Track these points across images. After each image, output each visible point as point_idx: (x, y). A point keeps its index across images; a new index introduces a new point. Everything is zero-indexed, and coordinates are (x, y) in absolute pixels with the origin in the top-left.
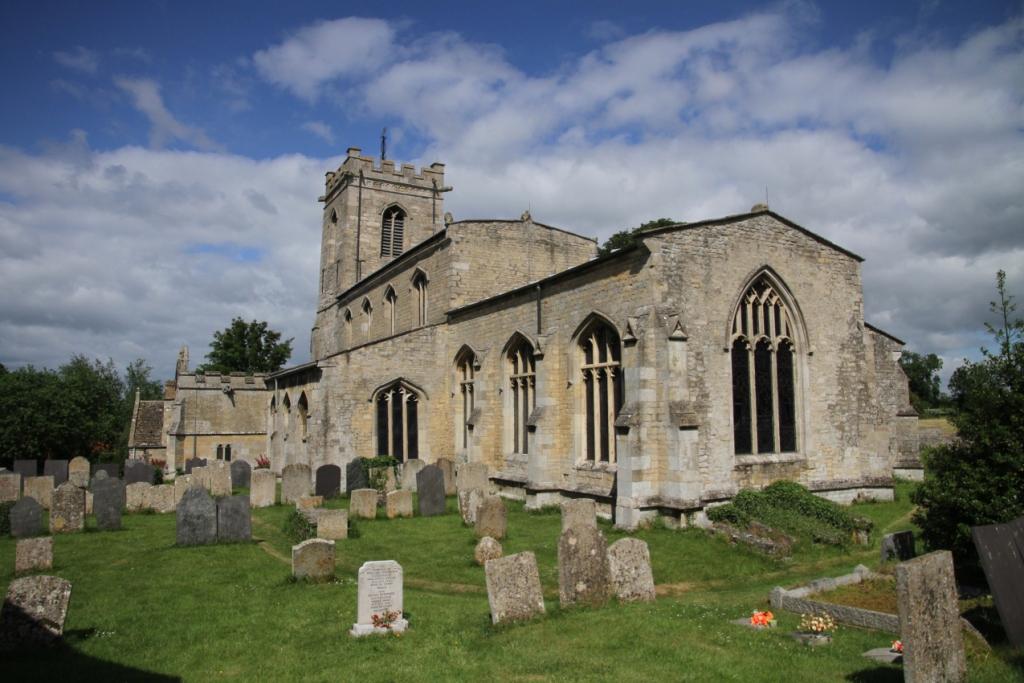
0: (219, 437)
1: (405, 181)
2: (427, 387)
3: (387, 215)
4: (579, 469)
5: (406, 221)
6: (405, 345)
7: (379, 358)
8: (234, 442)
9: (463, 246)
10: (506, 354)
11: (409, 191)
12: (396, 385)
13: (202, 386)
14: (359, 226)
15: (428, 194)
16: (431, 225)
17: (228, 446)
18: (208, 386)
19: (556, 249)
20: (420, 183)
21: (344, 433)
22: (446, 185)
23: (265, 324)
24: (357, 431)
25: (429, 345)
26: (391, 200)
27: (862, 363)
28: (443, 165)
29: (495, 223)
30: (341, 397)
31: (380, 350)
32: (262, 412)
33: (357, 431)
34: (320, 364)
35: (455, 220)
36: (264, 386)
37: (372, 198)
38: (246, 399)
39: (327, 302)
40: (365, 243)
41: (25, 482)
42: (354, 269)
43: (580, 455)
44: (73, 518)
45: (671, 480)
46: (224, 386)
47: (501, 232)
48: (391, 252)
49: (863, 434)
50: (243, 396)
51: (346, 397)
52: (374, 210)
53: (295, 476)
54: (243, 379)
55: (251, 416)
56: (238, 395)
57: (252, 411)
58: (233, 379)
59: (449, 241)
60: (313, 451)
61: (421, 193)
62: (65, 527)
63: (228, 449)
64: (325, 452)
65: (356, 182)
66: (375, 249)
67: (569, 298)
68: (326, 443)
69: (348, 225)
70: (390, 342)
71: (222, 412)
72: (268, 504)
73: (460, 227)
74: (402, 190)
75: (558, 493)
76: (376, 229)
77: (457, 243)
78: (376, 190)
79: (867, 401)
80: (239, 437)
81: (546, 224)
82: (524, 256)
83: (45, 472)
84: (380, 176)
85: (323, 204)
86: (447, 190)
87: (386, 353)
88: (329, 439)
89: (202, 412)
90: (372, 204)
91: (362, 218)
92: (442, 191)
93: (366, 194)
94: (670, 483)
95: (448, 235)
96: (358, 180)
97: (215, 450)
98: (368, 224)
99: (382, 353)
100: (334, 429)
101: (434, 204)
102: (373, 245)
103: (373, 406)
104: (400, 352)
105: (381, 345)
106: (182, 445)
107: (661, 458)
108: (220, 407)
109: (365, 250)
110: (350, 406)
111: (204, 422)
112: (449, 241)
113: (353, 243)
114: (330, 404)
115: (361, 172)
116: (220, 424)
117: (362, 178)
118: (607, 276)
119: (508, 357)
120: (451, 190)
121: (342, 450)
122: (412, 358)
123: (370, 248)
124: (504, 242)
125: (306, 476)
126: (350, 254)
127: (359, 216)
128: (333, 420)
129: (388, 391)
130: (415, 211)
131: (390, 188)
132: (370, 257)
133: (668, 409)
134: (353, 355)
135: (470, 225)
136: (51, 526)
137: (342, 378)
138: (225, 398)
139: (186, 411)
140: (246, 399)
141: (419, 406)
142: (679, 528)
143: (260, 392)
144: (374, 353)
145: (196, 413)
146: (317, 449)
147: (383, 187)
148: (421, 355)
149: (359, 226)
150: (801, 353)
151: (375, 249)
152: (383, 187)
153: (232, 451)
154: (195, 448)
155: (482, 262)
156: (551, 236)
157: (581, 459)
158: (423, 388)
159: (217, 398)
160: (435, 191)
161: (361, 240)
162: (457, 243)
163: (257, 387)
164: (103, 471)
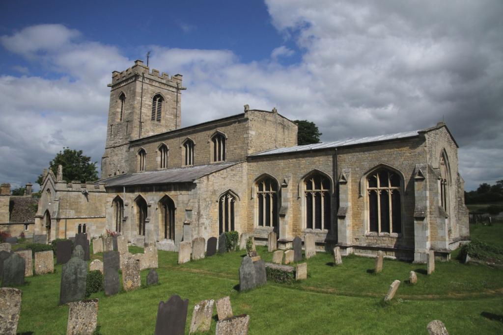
0: (80, 219)
1: (164, 81)
2: (239, 194)
3: (155, 99)
4: (367, 236)
5: (163, 103)
6: (230, 172)
7: (221, 179)
8: (88, 222)
9: (253, 122)
10: (304, 179)
11: (166, 87)
12: (227, 193)
13: (70, 189)
14: (141, 103)
15: (174, 90)
16: (175, 107)
17: (85, 224)
18: (74, 190)
19: (285, 127)
20: (171, 84)
21: (206, 219)
22: (183, 87)
23: (81, 152)
24: (212, 218)
25: (240, 172)
26: (157, 91)
27: (460, 190)
28: (182, 76)
29: (264, 113)
30: (205, 199)
31: (221, 175)
32: (103, 205)
33: (212, 218)
34: (196, 181)
35: (250, 109)
36: (105, 190)
37: (148, 89)
38: (94, 197)
39: (114, 143)
40: (144, 113)
41: (36, 255)
42: (138, 126)
43: (367, 229)
44: (135, 280)
45: (439, 240)
46: (82, 190)
47: (267, 117)
48: (156, 119)
49: (460, 218)
50: (93, 195)
51: (207, 200)
52: (149, 96)
53: (199, 244)
54: (93, 186)
55: (97, 207)
56: (91, 195)
57: (98, 205)
58: (88, 186)
59: (247, 119)
60: (193, 229)
61: (171, 89)
62: (132, 286)
63: (84, 226)
64: (199, 230)
65: (141, 79)
66: (149, 116)
67: (360, 156)
68: (199, 225)
69: (136, 102)
70: (225, 170)
71: (82, 205)
72: (187, 261)
73: (252, 113)
74: (162, 86)
75: (352, 248)
76: (150, 105)
77: (251, 121)
78: (150, 85)
79: (461, 205)
80: (90, 219)
81: (282, 115)
82: (274, 130)
83: (425, 269)
84: (152, 78)
85: (110, 89)
86: (183, 89)
87: (223, 176)
88: (200, 222)
89: (71, 205)
90: (148, 92)
91: (143, 99)
92: (181, 89)
93: (145, 86)
94: (439, 242)
95: (246, 116)
96: (142, 78)
97: (77, 227)
98: (146, 102)
99: (222, 176)
100: (203, 217)
101: (177, 96)
102: (148, 114)
103: (218, 204)
104: (229, 176)
105: (221, 172)
106: (58, 225)
107: (432, 231)
108: (80, 202)
109: (144, 116)
110: (209, 204)
111: (71, 211)
112: (247, 119)
113: (138, 112)
114: (200, 203)
115: (143, 74)
116: (80, 212)
117: (144, 77)
118: (392, 148)
119: (304, 181)
120: (185, 89)
121: (205, 228)
122: (233, 179)
123: (146, 116)
124: (268, 122)
125: (203, 243)
126: (136, 118)
127: (142, 98)
128: (202, 212)
129: (223, 196)
130: (168, 98)
131: (157, 84)
132: (146, 121)
133: (438, 209)
134: (210, 176)
135: (256, 112)
136: (125, 287)
137: (206, 189)
138: (83, 196)
139: (61, 204)
140: (94, 197)
141: (235, 204)
142: (22, 235)
143: (102, 193)
144: (218, 176)
145: (67, 205)
146: (195, 228)
147: (154, 84)
148: (237, 178)
149: (141, 103)
150: (448, 185)
151: (149, 116)
152: (154, 84)
153: (87, 227)
154: (66, 226)
155: (260, 131)
156: (283, 121)
157: (367, 231)
158: (238, 194)
159: (79, 197)
160: (178, 89)
161: (142, 111)
162: (251, 121)
163: (101, 191)
164: (80, 246)
